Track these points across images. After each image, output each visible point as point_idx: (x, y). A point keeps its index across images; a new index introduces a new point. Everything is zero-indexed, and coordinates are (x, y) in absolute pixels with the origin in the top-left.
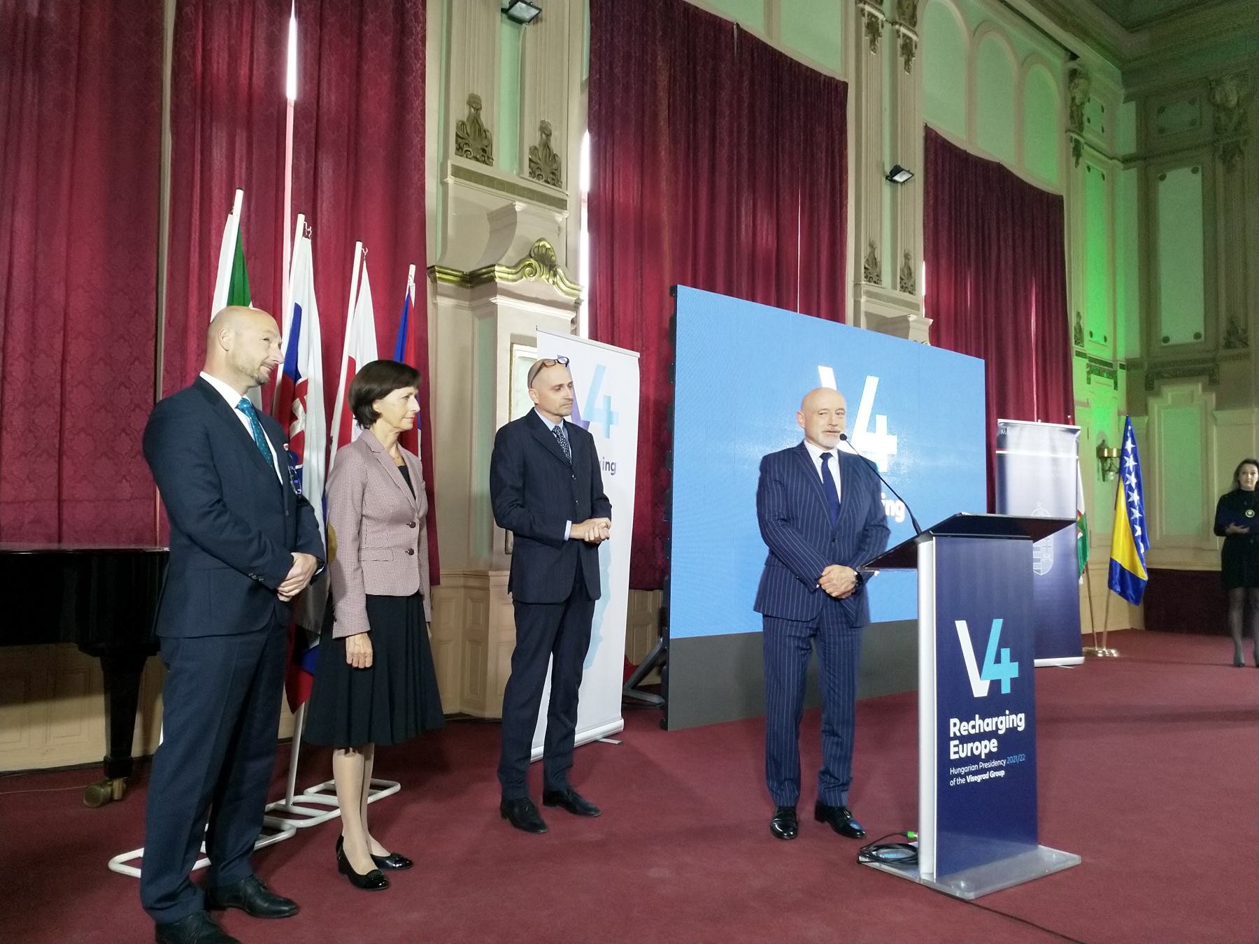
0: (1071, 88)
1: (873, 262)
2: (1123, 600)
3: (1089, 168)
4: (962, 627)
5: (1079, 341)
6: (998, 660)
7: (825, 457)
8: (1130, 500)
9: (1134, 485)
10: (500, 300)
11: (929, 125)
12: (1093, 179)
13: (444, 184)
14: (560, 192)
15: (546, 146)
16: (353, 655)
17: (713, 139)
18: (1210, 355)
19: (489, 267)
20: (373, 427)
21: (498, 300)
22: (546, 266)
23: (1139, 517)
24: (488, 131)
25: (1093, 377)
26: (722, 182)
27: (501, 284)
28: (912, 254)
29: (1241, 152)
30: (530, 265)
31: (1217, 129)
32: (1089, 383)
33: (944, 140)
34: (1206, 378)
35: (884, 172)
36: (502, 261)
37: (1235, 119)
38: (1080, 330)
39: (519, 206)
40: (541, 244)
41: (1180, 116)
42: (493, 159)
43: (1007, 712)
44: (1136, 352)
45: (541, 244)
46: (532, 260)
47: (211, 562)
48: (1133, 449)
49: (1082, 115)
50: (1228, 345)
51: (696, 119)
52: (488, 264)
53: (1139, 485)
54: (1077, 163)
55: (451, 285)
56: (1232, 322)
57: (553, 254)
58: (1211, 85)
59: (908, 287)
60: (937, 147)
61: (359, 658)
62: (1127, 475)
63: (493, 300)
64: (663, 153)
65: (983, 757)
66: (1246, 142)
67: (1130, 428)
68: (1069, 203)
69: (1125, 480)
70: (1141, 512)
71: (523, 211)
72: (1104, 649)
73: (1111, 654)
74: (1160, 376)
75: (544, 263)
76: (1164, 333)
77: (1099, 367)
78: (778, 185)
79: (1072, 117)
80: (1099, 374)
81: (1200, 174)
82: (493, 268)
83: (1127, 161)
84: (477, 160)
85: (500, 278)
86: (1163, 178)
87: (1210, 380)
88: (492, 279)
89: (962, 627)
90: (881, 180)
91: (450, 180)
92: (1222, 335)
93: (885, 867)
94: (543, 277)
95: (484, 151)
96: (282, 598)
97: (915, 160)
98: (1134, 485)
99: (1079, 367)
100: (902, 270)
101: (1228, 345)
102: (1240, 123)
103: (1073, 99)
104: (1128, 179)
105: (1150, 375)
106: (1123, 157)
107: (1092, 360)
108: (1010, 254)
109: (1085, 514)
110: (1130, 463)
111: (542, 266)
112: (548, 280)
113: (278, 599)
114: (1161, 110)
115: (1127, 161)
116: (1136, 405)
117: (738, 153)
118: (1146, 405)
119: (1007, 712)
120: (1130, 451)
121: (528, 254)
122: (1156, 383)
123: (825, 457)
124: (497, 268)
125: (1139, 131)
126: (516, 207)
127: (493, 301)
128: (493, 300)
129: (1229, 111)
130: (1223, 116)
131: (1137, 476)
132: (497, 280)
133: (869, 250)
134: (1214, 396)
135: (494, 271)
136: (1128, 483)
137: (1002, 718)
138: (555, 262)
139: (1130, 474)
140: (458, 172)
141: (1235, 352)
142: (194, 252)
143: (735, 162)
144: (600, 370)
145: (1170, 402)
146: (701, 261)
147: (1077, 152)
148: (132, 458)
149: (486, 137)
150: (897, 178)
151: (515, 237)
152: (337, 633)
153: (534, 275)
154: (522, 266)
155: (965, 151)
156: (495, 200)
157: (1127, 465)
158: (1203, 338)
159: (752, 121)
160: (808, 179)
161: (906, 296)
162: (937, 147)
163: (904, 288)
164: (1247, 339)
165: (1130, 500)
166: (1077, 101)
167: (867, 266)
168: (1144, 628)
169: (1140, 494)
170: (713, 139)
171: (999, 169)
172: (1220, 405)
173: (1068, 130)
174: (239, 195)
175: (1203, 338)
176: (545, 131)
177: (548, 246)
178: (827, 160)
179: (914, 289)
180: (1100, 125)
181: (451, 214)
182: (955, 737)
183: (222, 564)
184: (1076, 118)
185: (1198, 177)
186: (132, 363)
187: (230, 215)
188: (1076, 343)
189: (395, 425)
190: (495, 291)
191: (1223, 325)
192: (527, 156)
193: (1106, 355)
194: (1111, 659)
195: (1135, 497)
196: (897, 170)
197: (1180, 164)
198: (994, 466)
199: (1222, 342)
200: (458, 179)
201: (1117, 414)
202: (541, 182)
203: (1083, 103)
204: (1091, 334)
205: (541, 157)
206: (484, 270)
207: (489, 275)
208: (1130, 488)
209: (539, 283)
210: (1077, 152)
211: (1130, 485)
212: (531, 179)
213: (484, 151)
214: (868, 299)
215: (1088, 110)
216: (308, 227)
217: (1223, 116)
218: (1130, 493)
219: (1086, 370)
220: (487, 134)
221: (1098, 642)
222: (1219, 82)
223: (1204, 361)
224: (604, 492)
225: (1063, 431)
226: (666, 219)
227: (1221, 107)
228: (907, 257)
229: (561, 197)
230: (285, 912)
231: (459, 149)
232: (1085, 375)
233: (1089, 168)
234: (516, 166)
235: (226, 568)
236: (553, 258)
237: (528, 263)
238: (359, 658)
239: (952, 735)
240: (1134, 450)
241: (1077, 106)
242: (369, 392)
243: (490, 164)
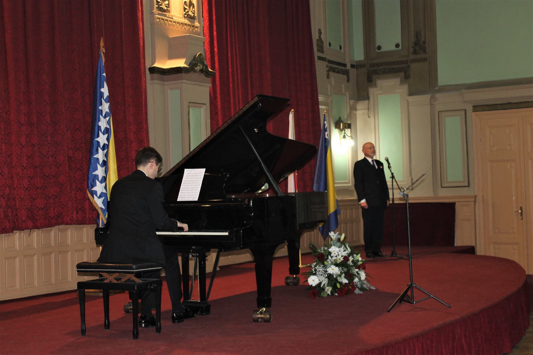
2: (97, 259)
5: (321, 49)
25: (331, 74)
34: (402, 74)
74: (376, 72)
76: (378, 44)
87: (405, 75)
99: (321, 68)
101: (415, 52)
107: (330, 62)
109: (336, 212)
122: (374, 77)
141: (419, 56)
142: (147, 71)
148: (5, 187)
158: (377, 51)
191: (413, 39)
198: (353, 179)
199: (412, 50)
223: (402, 62)
224: (248, 249)
227: (205, 71)
232: (325, 73)
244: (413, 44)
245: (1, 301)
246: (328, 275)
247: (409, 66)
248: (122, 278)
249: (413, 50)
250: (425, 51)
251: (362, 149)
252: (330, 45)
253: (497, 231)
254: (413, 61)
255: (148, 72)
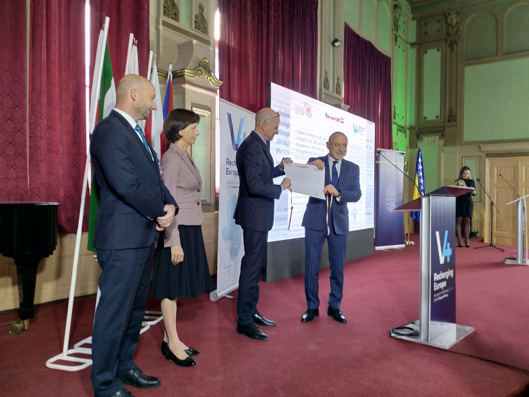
0: (394, 12)
1: (327, 80)
3: (399, 47)
4: (437, 233)
5: (395, 118)
6: (446, 248)
7: (335, 163)
8: (420, 182)
9: (421, 176)
10: (187, 86)
11: (346, 22)
12: (401, 50)
13: (158, 29)
14: (207, 37)
15: (202, 15)
16: (175, 256)
17: (268, 19)
18: (442, 125)
19: (181, 70)
20: (177, 143)
21: (186, 86)
22: (207, 71)
23: (423, 189)
24: (177, 5)
25: (399, 132)
26: (272, 39)
27: (187, 78)
28: (340, 77)
29: (457, 44)
30: (200, 70)
31: (448, 34)
32: (397, 135)
33: (351, 30)
34: (440, 134)
35: (331, 42)
36: (187, 67)
37: (455, 30)
38: (395, 113)
39: (195, 42)
40: (205, 60)
41: (434, 27)
42: (179, 19)
43: (449, 270)
44: (413, 123)
45: (205, 60)
46: (201, 68)
47: (129, 210)
48: (421, 162)
49: (398, 24)
50: (449, 121)
51: (262, 9)
52: (182, 68)
53: (423, 176)
54: (396, 44)
55: (162, 77)
56: (451, 111)
57: (209, 65)
58: (446, 15)
59: (338, 92)
60: (348, 31)
61: (178, 257)
62: (419, 172)
63: (183, 86)
64: (249, 24)
65: (442, 289)
66: (458, 40)
67: (420, 153)
68: (393, 61)
69: (418, 174)
70: (424, 187)
71: (196, 44)
72: (409, 241)
73: (411, 243)
74: (422, 132)
75: (206, 70)
77: (401, 129)
78: (292, 42)
79: (394, 24)
80: (401, 131)
81: (440, 51)
82: (184, 71)
83: (412, 45)
84: (172, 18)
85: (187, 75)
86: (426, 52)
87: (441, 135)
88: (183, 76)
89: (437, 233)
90: (330, 44)
91: (161, 27)
92: (447, 117)
93: (404, 338)
94: (206, 76)
95: (176, 14)
96: (158, 228)
97: (341, 36)
98: (421, 176)
99: (394, 127)
100: (337, 85)
102: (457, 32)
103: (395, 17)
104: (412, 52)
105: (419, 133)
106: (411, 43)
107: (399, 126)
108: (373, 80)
110: (420, 167)
111: (205, 71)
112: (207, 78)
113: (156, 228)
114: (426, 24)
115: (412, 45)
116: (412, 145)
117: (278, 26)
118: (417, 145)
119: (449, 270)
120: (420, 162)
121: (198, 64)
122: (421, 135)
123: (335, 163)
124: (186, 70)
125: (417, 33)
126: (193, 42)
127: (184, 86)
128: (183, 86)
129: (453, 27)
130: (450, 28)
131: (423, 172)
132: (185, 76)
133: (325, 75)
134: (443, 141)
135: (185, 72)
136: (419, 175)
137: (447, 272)
138: (210, 69)
139: (420, 171)
140: (165, 24)
143: (277, 31)
144: (242, 120)
145: (426, 143)
146: (264, 74)
147: (396, 40)
149: (176, 8)
150: (336, 44)
151: (193, 56)
152: (166, 245)
153: (202, 75)
154: (197, 70)
155: (359, 35)
156: (182, 39)
157: (419, 168)
158: (424, 120)
159: (283, 14)
160: (303, 42)
161: (338, 96)
162: (348, 31)
163: (337, 92)
164: (456, 119)
165: (420, 182)
166: (397, 18)
167: (324, 81)
168: (414, 233)
169: (423, 180)
170: (268, 19)
171: (370, 43)
172: (445, 145)
173: (392, 30)
174: (107, 19)
175: (439, 118)
176: (201, 8)
177: (208, 62)
178: (310, 34)
179: (341, 93)
180: (403, 29)
181: (161, 43)
182: (436, 281)
183: (135, 212)
184: (396, 26)
185: (440, 53)
186: (15, 109)
187: (101, 30)
188: (394, 118)
189: (188, 142)
190: (184, 82)
191: (447, 113)
192: (194, 19)
193: (402, 124)
194: (411, 245)
195: (422, 181)
196: (336, 41)
197: (432, 47)
199: (447, 120)
200: (165, 27)
201: (406, 147)
202: (200, 31)
203: (398, 19)
204: (398, 115)
205: (199, 20)
206: (179, 71)
207: (182, 74)
208: (420, 177)
209: (204, 78)
210: (396, 40)
211: (420, 176)
212: (196, 30)
213: (176, 14)
214: (325, 96)
215: (400, 23)
216: (136, 40)
217: (450, 28)
218: (420, 179)
219: (396, 129)
220: (177, 6)
221: (406, 239)
222: (449, 14)
223: (440, 127)
225: (400, 154)
226: (250, 54)
227: (448, 25)
228: (338, 79)
229: (208, 39)
230: (156, 384)
231: (165, 13)
233: (399, 47)
234: (189, 23)
235: (133, 213)
236: (210, 67)
237: (199, 69)
238: (178, 257)
239: (434, 280)
240: (422, 162)
241: (396, 20)
242: (178, 126)
243: (178, 21)
244: (448, 116)
245: (528, 156)
246: (193, 364)
247: (444, 129)
248: (395, 209)
249: (448, 119)
250: (456, 121)
251: (362, 192)
252: (398, 115)
253: (499, 229)
254: (448, 126)
255: (393, 123)
